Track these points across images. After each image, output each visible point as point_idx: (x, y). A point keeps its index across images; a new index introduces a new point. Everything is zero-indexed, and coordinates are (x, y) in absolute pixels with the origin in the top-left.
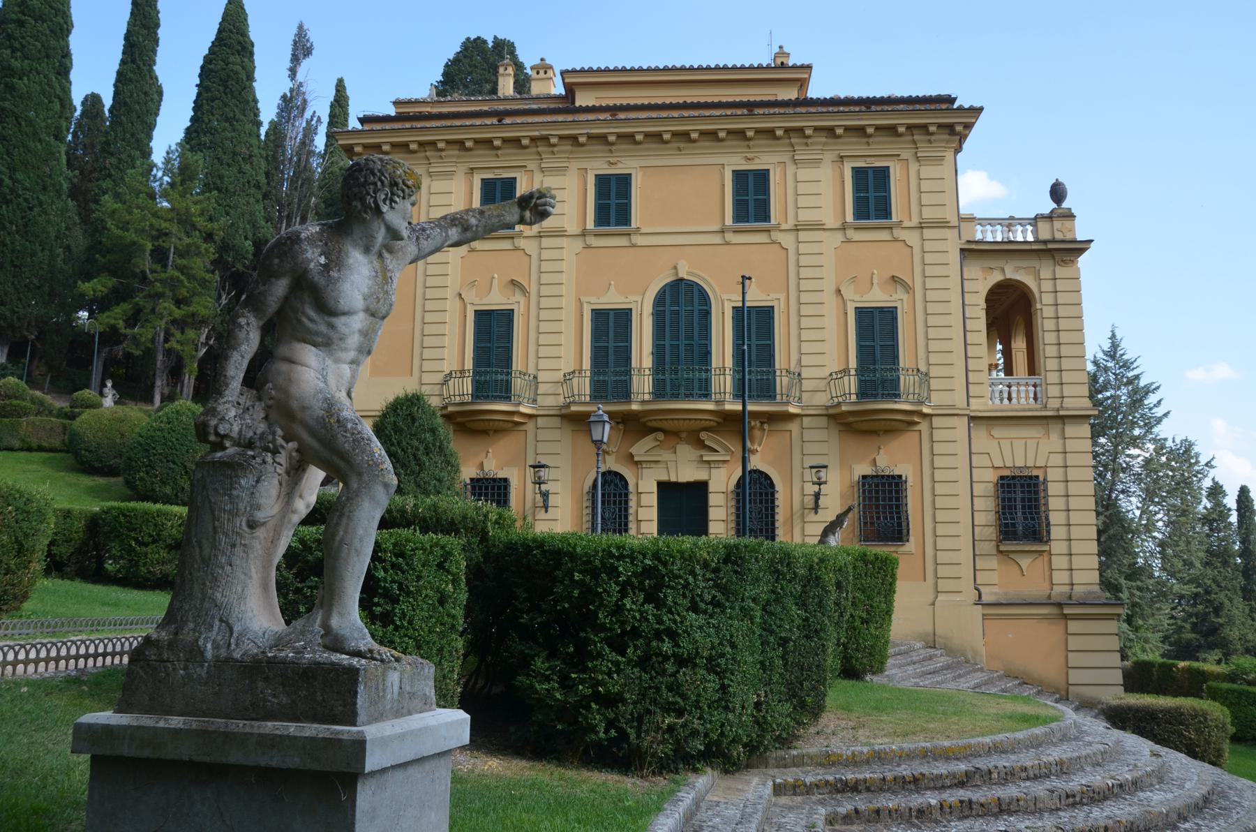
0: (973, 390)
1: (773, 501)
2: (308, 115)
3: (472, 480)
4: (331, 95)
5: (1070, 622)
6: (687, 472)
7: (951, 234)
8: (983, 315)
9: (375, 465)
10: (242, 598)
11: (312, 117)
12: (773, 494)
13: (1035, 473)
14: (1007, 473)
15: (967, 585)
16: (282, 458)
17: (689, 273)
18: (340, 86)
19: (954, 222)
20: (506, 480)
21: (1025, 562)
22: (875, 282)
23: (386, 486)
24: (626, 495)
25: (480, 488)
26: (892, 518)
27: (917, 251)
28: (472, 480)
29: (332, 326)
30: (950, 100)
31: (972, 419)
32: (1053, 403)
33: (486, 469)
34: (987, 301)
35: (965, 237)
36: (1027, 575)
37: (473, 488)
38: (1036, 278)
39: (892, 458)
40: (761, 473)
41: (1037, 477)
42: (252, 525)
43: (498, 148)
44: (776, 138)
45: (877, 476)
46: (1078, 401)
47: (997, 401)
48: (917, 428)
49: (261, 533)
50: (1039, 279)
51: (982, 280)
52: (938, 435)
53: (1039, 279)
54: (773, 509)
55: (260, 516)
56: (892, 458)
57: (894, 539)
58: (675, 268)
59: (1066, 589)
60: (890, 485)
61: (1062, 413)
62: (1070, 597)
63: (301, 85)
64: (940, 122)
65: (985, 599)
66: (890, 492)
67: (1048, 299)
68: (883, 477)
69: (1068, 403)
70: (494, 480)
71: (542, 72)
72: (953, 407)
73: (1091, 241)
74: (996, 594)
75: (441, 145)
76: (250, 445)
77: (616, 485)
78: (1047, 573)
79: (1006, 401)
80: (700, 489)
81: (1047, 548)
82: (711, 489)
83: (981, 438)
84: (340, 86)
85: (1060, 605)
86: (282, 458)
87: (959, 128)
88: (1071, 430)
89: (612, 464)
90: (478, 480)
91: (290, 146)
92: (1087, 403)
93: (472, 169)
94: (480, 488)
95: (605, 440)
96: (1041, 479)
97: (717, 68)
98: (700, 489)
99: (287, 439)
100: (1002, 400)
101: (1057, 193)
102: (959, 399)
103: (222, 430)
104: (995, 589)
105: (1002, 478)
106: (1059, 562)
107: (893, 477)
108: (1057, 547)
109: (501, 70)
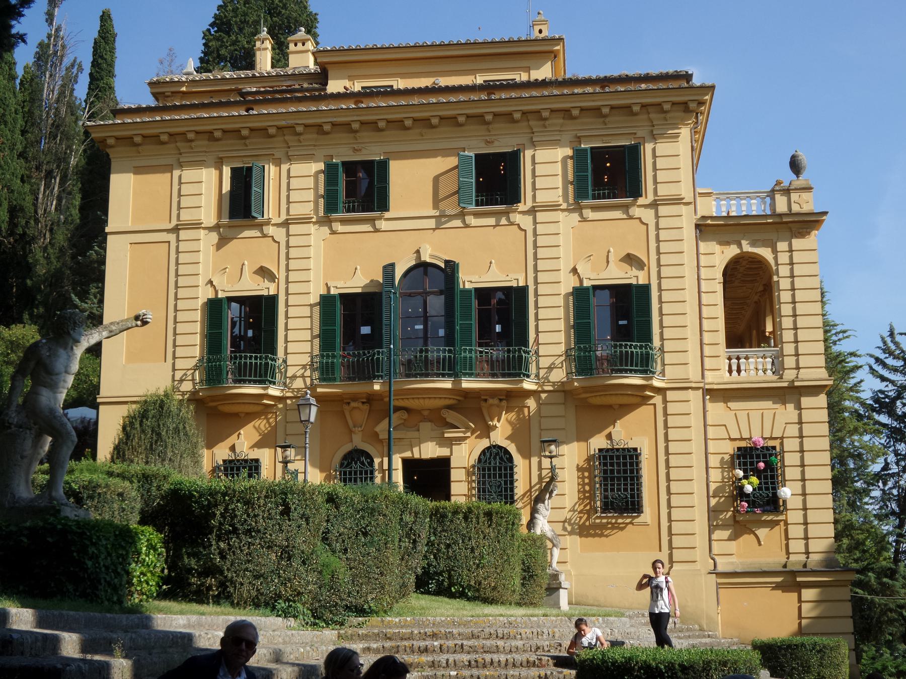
0: (708, 363)
1: (512, 475)
2: (67, 61)
3: (224, 461)
4: (93, 31)
5: (803, 591)
6: (430, 450)
7: (684, 210)
8: (720, 288)
9: (69, 433)
10: (18, 485)
11: (73, 65)
12: (512, 469)
13: (771, 443)
14: (743, 444)
15: (700, 553)
16: (33, 432)
17: (432, 256)
18: (105, 18)
19: (688, 197)
20: (257, 461)
21: (762, 532)
22: (611, 259)
23: (73, 441)
24: (372, 472)
25: (232, 469)
26: (626, 490)
27: (652, 228)
28: (224, 461)
29: (52, 380)
30: (688, 77)
31: (709, 392)
32: (789, 375)
33: (238, 451)
34: (725, 274)
35: (700, 214)
36: (764, 548)
37: (226, 469)
38: (774, 255)
39: (629, 432)
40: (500, 448)
41: (774, 448)
42: (22, 457)
43: (245, 138)
44: (514, 121)
45: (612, 449)
46: (814, 370)
47: (753, 372)
48: (651, 402)
49: (26, 460)
50: (775, 252)
51: (719, 255)
52: (671, 408)
53: (775, 252)
54: (512, 482)
55: (25, 454)
56: (629, 432)
57: (627, 510)
58: (418, 252)
59: (803, 558)
60: (625, 457)
61: (796, 384)
62: (805, 566)
63: (58, 30)
64: (676, 99)
65: (720, 569)
66: (625, 464)
67: (784, 271)
68: (618, 450)
69: (803, 374)
70: (246, 461)
71: (300, 45)
72: (687, 380)
73: (825, 213)
74: (732, 563)
75: (191, 136)
76: (21, 427)
77: (363, 463)
78: (784, 542)
79: (735, 373)
80: (443, 464)
81: (780, 518)
82: (453, 464)
83: (716, 410)
84: (105, 18)
85: (794, 574)
86: (33, 432)
87: (692, 105)
88: (806, 401)
89: (358, 442)
90: (231, 461)
91: (49, 92)
92: (823, 373)
93: (221, 158)
94: (232, 469)
95: (312, 419)
96: (778, 449)
97: (467, 44)
98: (443, 464)
99: (35, 424)
100: (730, 371)
101: (795, 166)
102: (693, 373)
103: (10, 421)
104: (733, 559)
105: (739, 449)
106: (796, 531)
107: (629, 450)
108: (795, 517)
109: (258, 44)
